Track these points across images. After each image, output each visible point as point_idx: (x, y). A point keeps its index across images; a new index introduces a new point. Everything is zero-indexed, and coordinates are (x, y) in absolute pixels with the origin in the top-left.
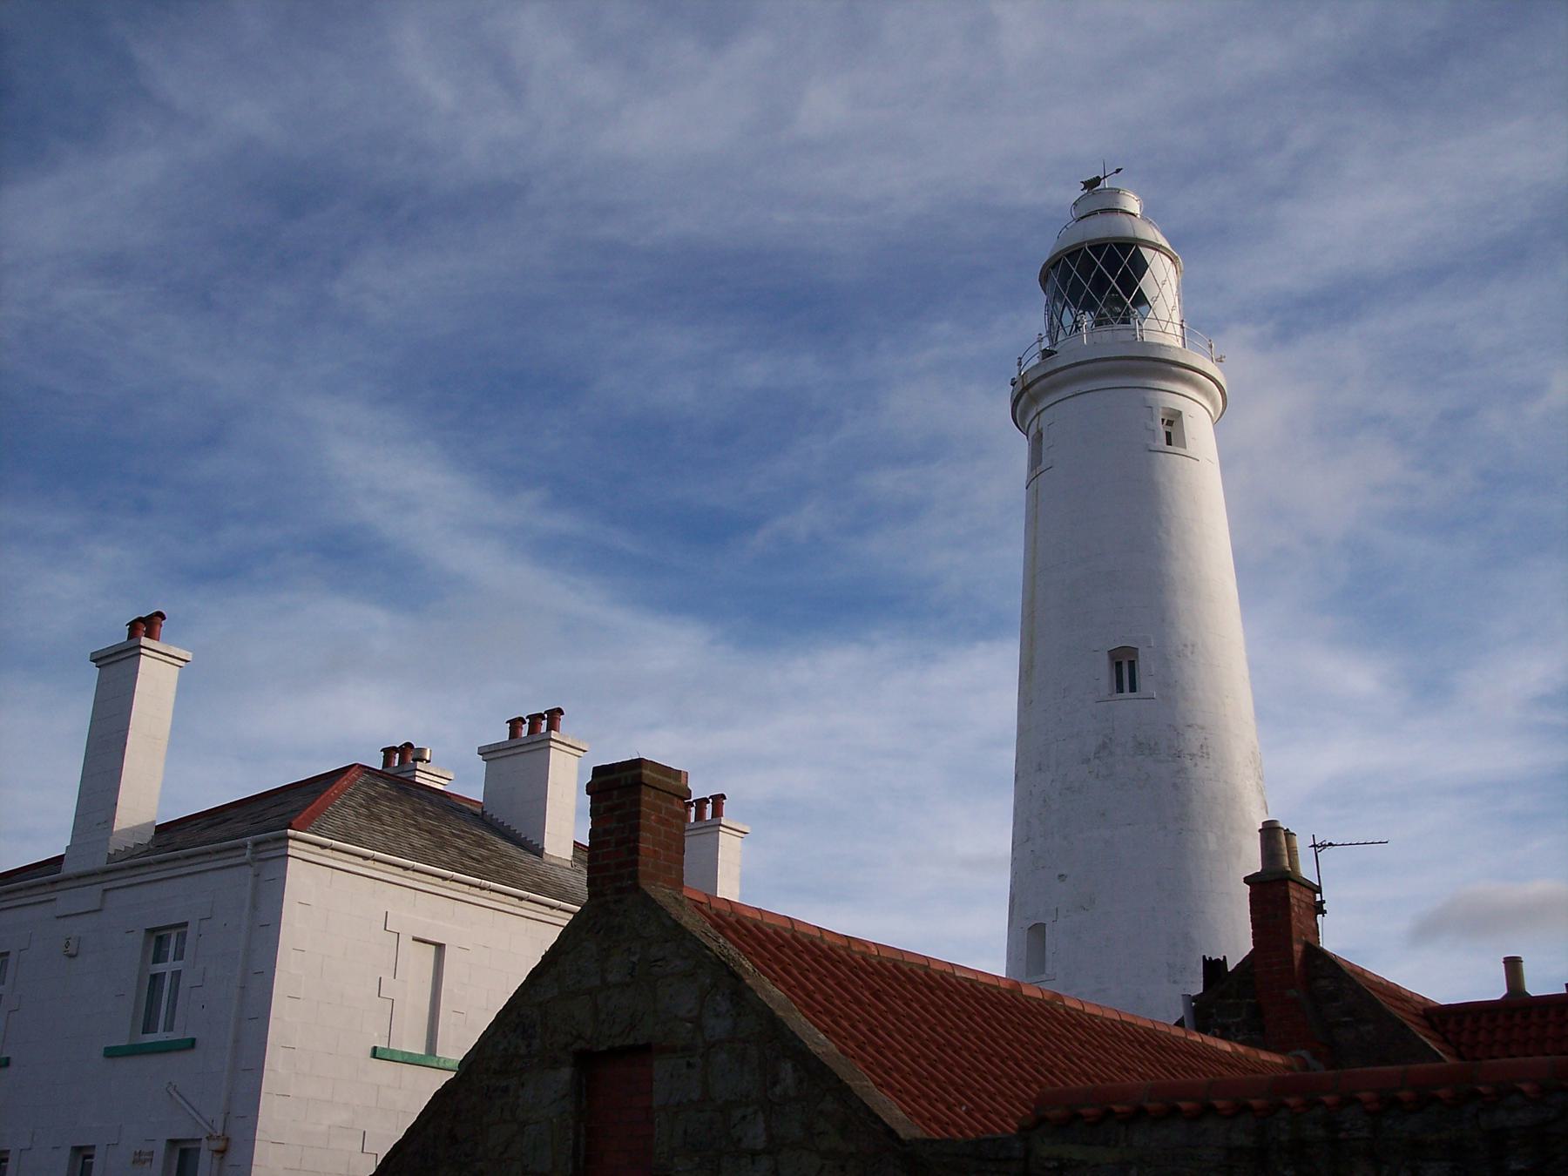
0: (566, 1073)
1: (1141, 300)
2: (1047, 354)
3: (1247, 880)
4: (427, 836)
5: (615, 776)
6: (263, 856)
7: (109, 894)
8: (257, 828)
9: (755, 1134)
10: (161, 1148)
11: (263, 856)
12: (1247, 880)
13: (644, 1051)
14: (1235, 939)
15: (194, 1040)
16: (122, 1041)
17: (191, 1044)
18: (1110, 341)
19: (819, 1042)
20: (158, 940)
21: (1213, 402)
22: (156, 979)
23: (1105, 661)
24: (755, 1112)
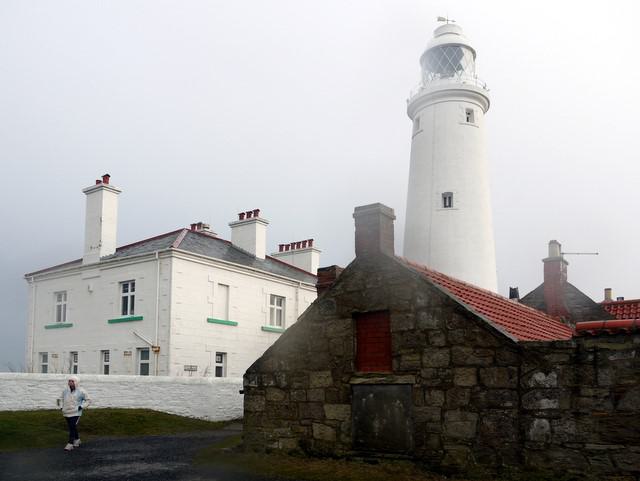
1: (460, 68)
2: (423, 89)
8: (158, 247)
10: (134, 351)
13: (387, 312)
17: (70, 325)
18: (453, 82)
20: (60, 295)
21: (485, 106)
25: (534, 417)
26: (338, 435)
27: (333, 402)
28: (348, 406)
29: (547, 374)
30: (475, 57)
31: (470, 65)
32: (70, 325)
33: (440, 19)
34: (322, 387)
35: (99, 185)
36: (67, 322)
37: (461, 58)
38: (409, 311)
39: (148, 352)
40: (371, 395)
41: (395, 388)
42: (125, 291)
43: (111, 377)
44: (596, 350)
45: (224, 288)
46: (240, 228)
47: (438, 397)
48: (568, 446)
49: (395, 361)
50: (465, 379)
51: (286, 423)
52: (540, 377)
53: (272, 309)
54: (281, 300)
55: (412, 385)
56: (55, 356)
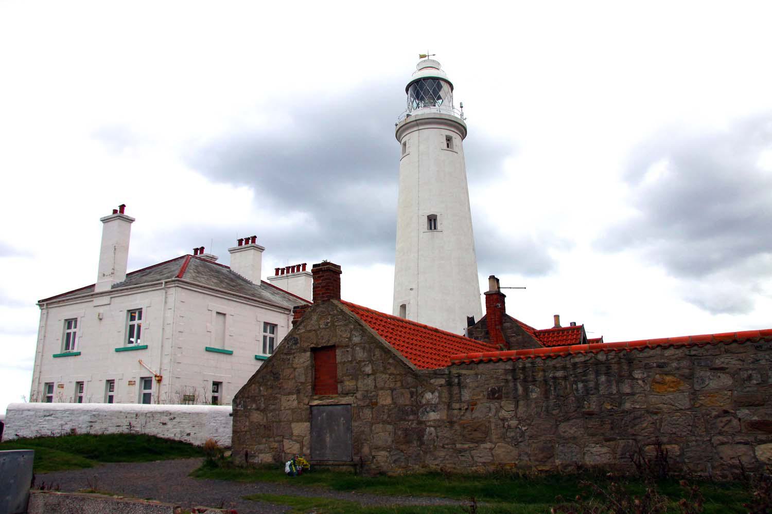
0: (308, 354)
3: (485, 294)
4: (216, 278)
5: (320, 267)
6: (168, 286)
7: (113, 299)
9: (368, 369)
10: (138, 381)
11: (168, 286)
12: (485, 294)
13: (333, 348)
14: (482, 311)
15: (147, 346)
16: (122, 346)
17: (79, 354)
19: (386, 343)
21: (462, 134)
22: (132, 327)
23: (426, 220)
24: (368, 364)
25: (426, 426)
26: (301, 448)
27: (298, 421)
28: (308, 424)
29: (432, 393)
30: (452, 89)
31: (448, 96)
32: (79, 354)
33: (422, 57)
34: (290, 409)
35: (116, 215)
36: (75, 351)
37: (440, 90)
38: (347, 346)
39: (151, 380)
40: (324, 414)
41: (339, 407)
42: (133, 318)
43: (114, 406)
44: (459, 376)
45: (221, 317)
46: (238, 254)
47: (368, 413)
48: (446, 446)
49: (339, 386)
50: (385, 400)
51: (264, 440)
52: (429, 396)
53: (265, 337)
54: (273, 327)
55: (350, 404)
56: (61, 386)
